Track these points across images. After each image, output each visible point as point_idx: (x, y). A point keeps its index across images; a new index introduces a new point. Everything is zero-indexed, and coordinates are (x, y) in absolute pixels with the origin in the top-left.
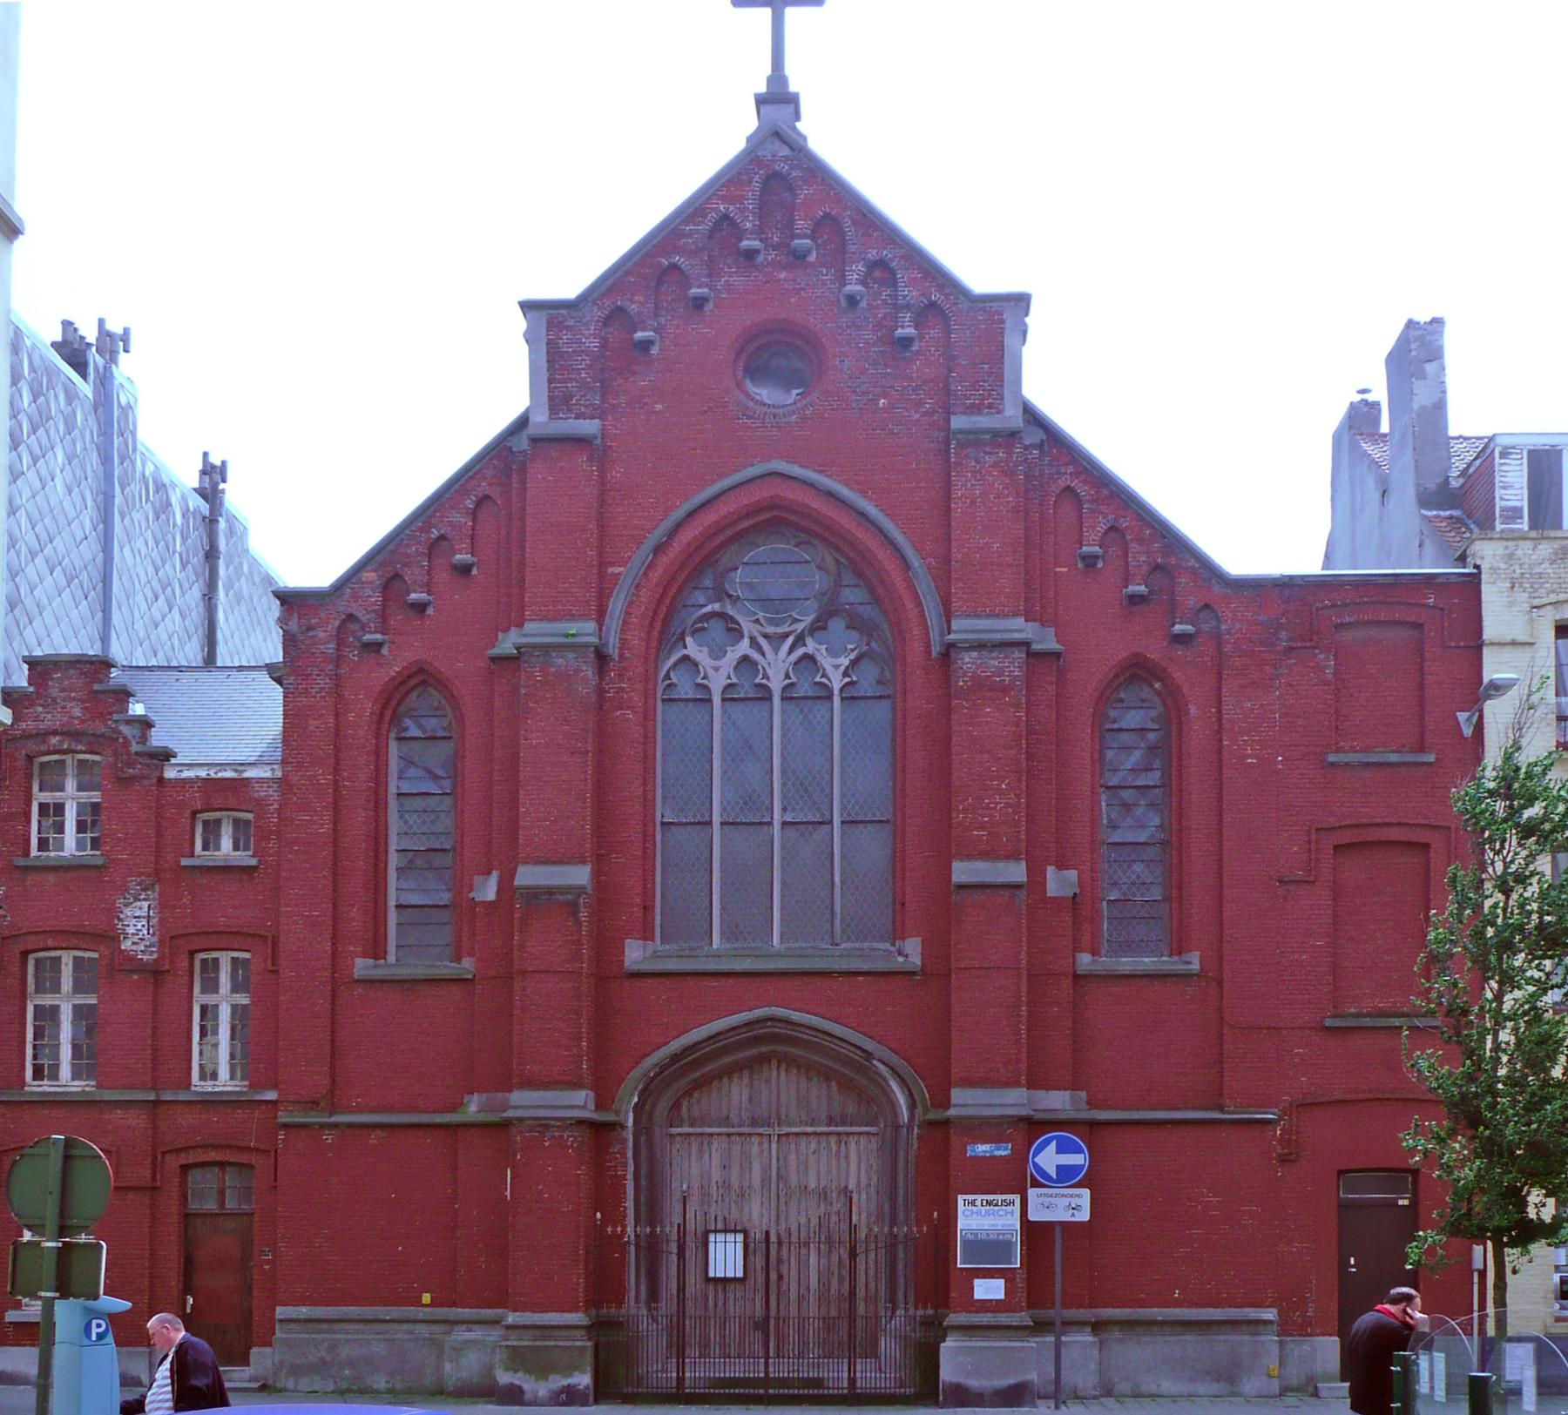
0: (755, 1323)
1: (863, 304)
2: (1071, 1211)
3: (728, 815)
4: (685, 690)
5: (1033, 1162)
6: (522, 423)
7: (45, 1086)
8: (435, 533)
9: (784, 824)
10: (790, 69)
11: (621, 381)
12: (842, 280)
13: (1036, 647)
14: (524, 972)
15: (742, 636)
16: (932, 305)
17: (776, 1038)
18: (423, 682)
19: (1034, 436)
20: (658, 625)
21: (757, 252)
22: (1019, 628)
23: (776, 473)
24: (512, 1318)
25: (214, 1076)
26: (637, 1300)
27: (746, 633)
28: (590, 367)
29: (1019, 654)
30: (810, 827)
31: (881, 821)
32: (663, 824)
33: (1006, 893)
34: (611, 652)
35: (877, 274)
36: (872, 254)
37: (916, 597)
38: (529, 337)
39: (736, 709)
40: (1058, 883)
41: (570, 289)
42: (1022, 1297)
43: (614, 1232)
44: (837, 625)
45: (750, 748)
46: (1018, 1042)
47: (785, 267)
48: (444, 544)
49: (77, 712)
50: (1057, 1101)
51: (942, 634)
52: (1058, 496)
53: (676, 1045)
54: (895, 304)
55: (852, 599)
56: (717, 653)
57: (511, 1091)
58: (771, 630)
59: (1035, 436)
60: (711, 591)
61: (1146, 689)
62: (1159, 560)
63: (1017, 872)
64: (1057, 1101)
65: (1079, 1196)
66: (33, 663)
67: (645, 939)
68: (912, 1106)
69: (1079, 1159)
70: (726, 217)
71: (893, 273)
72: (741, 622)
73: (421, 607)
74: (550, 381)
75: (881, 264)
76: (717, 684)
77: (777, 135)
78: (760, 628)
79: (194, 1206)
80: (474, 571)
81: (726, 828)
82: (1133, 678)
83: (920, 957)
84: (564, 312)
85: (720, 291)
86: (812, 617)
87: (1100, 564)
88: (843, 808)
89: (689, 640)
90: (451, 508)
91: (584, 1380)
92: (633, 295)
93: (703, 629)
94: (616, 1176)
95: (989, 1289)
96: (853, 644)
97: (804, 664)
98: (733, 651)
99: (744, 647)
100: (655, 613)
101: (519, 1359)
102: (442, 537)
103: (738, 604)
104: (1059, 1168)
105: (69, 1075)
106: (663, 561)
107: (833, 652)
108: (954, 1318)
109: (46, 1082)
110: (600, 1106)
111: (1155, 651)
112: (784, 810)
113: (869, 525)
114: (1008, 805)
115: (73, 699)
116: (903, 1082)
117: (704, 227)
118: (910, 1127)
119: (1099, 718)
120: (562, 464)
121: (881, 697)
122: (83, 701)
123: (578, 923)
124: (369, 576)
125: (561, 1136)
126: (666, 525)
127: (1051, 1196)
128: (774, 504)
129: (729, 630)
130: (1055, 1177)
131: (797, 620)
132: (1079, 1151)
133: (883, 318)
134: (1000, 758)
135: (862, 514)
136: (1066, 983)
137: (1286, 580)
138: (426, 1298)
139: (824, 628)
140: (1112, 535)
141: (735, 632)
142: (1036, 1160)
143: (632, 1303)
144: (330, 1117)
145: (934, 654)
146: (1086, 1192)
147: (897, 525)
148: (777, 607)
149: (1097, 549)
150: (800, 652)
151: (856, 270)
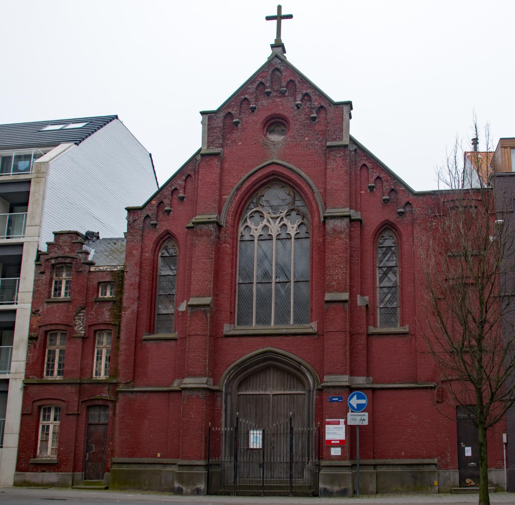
0: (260, 465)
1: (302, 108)
2: (362, 421)
3: (259, 280)
4: (247, 237)
5: (349, 403)
6: (200, 150)
7: (50, 378)
8: (173, 188)
9: (276, 283)
10: (283, 38)
11: (229, 136)
12: (295, 100)
13: (353, 218)
14: (190, 335)
15: (264, 218)
16: (322, 107)
17: (272, 359)
18: (169, 237)
19: (353, 148)
20: (238, 215)
21: (270, 93)
22: (346, 211)
23: (274, 163)
24: (180, 462)
25: (100, 374)
26: (225, 456)
27: (265, 217)
28: (220, 131)
29: (347, 220)
30: (284, 283)
31: (306, 281)
32: (239, 284)
33: (342, 304)
34: (222, 224)
35: (306, 98)
36: (304, 92)
37: (315, 199)
38: (202, 123)
39: (263, 243)
40: (361, 301)
41: (214, 107)
42: (348, 455)
43: (218, 430)
44: (294, 213)
45: (266, 256)
46: (346, 358)
47: (279, 97)
48: (176, 191)
49: (67, 250)
50: (361, 381)
51: (323, 214)
52: (361, 167)
53: (238, 361)
54: (311, 107)
55: (298, 205)
56: (257, 224)
57: (184, 378)
58: (273, 216)
59: (353, 148)
60: (255, 204)
61: (391, 232)
62: (393, 187)
63: (345, 296)
64: (361, 381)
65: (364, 415)
66: (56, 234)
67: (231, 323)
68: (314, 384)
69: (363, 401)
70: (261, 83)
71: (310, 97)
72: (264, 213)
73: (169, 211)
74: (208, 136)
75: (307, 94)
76: (256, 234)
77: (277, 56)
78: (269, 215)
79: (91, 421)
80: (185, 200)
81: (258, 284)
82: (386, 229)
83: (316, 328)
84: (213, 115)
85: (259, 106)
86: (286, 211)
87: (375, 190)
88: (295, 276)
89: (248, 220)
90: (179, 179)
91: (202, 486)
92: (233, 108)
93: (253, 216)
94: (218, 410)
95: (336, 452)
96: (299, 220)
97: (283, 227)
98: (262, 224)
99: (265, 222)
100: (237, 211)
101: (180, 477)
102: (176, 189)
103: (264, 207)
104: (358, 405)
105: (57, 374)
106: (240, 193)
107: (292, 223)
108: (323, 463)
109: (50, 377)
110: (214, 384)
111: (393, 218)
112: (276, 277)
113: (302, 179)
114: (343, 273)
115: (66, 246)
116: (311, 374)
117: (255, 86)
118: (313, 391)
119: (375, 242)
120: (210, 163)
121: (307, 238)
122: (69, 246)
123: (207, 317)
124: (154, 202)
125: (198, 394)
126: (241, 181)
127: (355, 415)
128: (274, 173)
129: (261, 216)
130: (356, 408)
131: (281, 212)
132: (364, 398)
133: (308, 112)
134: (341, 256)
135: (290, 169)
136: (364, 337)
137: (433, 192)
138: (159, 455)
139: (290, 215)
140: (378, 180)
141: (262, 216)
142: (350, 402)
143: (223, 457)
144: (133, 388)
145: (321, 222)
146: (366, 414)
147: (311, 178)
148: (275, 209)
149: (373, 184)
150: (282, 223)
151: (299, 97)
